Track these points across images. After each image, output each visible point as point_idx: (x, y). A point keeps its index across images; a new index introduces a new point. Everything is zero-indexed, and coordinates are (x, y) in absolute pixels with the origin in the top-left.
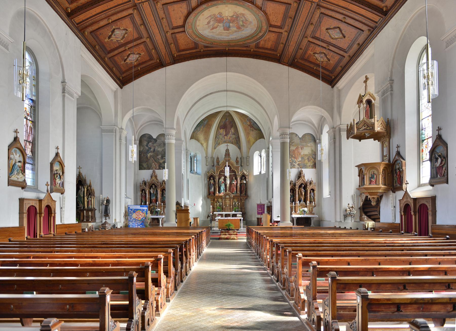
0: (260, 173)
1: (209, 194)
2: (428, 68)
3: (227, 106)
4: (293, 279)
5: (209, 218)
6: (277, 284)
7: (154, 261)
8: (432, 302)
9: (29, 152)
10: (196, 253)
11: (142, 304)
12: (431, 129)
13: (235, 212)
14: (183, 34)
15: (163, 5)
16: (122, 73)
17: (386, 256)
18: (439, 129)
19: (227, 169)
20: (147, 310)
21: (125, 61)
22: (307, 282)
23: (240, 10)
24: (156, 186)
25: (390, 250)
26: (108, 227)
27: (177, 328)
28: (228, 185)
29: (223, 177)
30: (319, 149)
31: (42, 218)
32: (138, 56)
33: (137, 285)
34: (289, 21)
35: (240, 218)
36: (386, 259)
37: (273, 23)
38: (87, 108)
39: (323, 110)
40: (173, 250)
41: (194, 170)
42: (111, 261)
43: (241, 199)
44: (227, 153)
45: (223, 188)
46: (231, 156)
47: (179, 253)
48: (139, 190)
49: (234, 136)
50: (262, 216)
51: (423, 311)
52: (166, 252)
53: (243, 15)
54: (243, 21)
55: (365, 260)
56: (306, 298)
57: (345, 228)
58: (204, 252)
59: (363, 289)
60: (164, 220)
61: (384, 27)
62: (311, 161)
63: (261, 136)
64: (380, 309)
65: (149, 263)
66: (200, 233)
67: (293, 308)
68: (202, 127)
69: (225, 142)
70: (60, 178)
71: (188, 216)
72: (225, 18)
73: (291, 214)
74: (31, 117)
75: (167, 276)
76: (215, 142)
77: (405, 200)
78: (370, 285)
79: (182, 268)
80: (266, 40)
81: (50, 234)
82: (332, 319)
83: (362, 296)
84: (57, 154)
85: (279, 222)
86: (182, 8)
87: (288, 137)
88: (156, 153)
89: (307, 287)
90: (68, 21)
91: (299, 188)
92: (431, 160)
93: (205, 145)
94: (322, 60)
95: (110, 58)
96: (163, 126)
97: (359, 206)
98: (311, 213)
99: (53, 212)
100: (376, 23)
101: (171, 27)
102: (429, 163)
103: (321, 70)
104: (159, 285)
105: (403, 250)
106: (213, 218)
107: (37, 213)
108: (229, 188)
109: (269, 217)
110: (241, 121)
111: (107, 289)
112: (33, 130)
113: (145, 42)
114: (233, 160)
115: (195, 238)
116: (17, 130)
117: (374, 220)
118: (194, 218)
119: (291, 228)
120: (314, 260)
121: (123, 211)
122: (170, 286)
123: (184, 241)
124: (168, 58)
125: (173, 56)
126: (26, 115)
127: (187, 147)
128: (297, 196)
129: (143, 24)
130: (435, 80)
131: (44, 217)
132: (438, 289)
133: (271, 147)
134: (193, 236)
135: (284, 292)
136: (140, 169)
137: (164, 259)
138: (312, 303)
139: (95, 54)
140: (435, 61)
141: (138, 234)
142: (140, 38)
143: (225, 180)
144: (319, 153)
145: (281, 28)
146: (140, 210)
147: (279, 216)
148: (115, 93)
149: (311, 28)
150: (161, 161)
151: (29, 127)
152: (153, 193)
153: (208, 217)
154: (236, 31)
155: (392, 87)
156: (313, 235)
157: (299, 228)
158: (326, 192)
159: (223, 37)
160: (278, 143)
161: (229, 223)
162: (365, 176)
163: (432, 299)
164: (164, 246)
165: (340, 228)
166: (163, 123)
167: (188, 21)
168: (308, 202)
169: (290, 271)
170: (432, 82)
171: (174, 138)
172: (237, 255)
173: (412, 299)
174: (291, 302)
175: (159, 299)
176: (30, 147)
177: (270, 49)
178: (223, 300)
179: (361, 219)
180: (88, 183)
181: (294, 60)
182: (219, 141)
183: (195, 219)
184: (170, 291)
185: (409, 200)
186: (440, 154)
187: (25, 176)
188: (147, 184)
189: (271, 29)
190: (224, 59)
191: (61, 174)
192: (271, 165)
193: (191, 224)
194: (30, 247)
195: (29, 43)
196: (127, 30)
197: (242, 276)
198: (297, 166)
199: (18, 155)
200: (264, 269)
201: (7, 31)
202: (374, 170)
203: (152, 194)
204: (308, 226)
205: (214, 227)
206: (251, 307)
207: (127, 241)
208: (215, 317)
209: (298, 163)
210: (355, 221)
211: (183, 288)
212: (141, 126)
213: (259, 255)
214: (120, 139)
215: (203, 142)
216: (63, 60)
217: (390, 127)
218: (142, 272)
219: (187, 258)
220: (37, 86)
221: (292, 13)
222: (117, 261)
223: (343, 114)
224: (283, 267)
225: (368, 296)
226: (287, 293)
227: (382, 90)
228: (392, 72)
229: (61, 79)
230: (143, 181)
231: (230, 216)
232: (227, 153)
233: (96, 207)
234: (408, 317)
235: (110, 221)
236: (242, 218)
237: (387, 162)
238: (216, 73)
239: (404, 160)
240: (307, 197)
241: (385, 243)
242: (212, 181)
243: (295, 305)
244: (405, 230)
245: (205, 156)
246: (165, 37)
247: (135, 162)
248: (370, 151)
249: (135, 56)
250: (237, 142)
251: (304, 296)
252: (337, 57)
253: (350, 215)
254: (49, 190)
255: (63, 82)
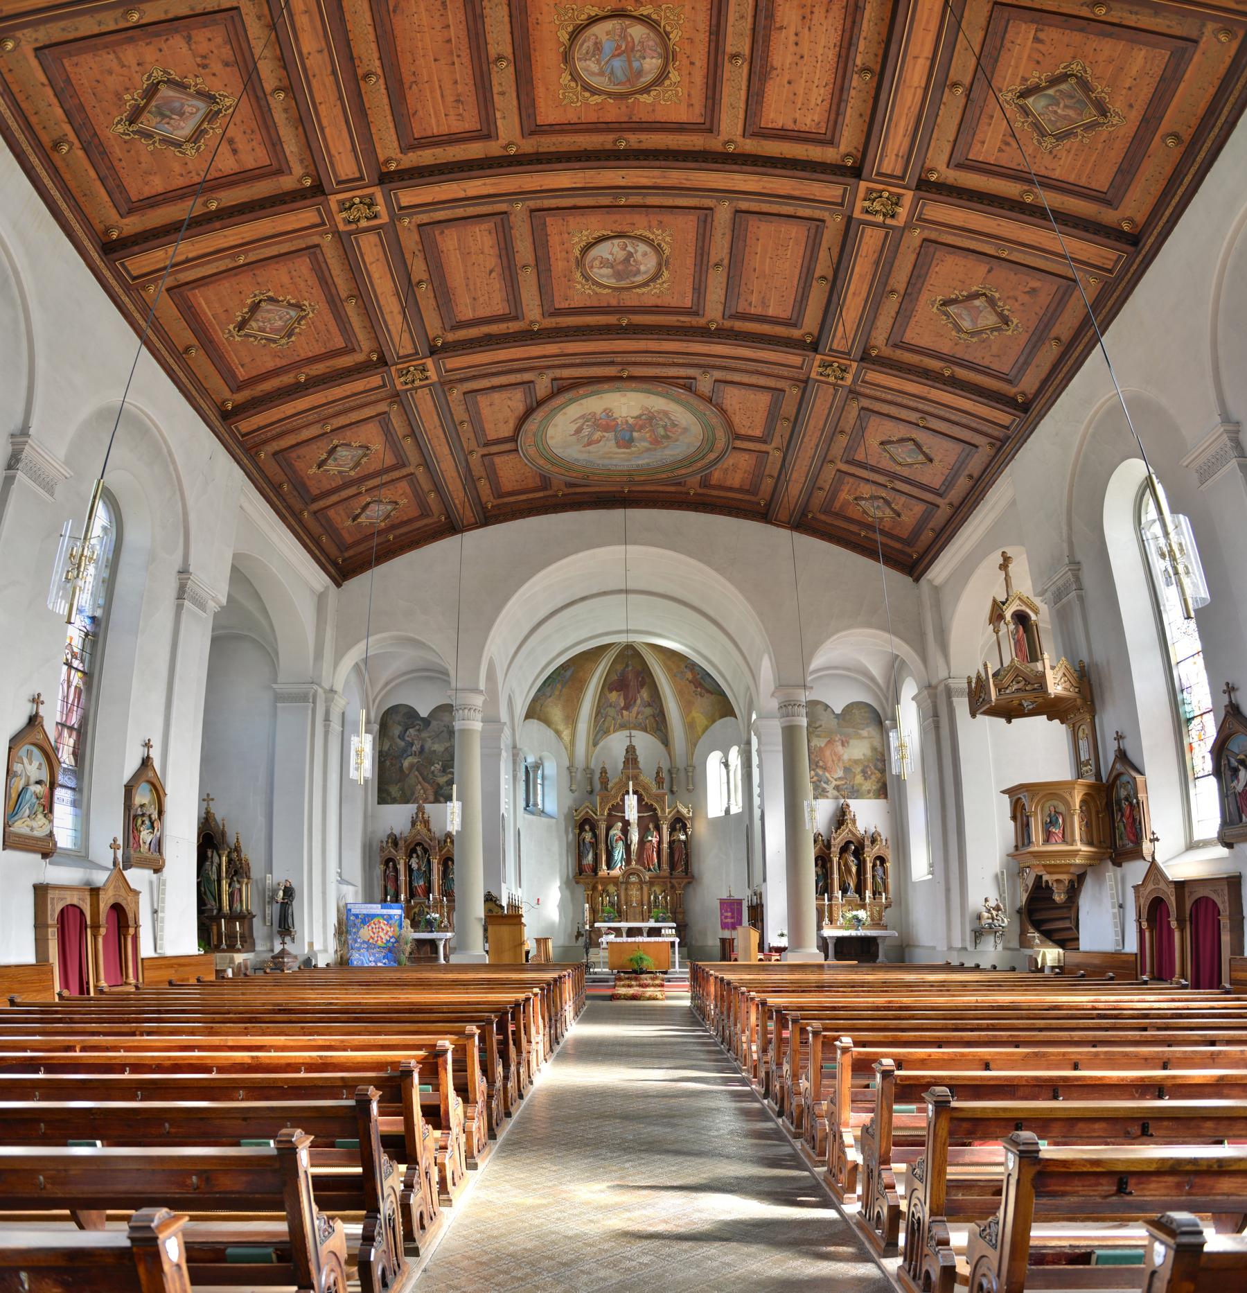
0: (727, 811)
1: (580, 870)
2: (1166, 534)
3: (627, 631)
4: (825, 1107)
5: (582, 940)
6: (780, 1121)
7: (426, 1058)
8: (1221, 1168)
9: (66, 757)
10: (547, 1038)
11: (401, 1175)
12: (1207, 689)
13: (657, 921)
14: (512, 456)
15: (465, 393)
16: (343, 547)
17: (1094, 1044)
18: (1230, 689)
19: (631, 802)
20: (415, 1190)
21: (354, 520)
22: (866, 1118)
23: (657, 403)
24: (425, 851)
25: (1107, 1029)
26: (292, 966)
27: (502, 1235)
28: (634, 847)
29: (620, 824)
30: (894, 743)
31: (100, 940)
32: (389, 507)
33: (382, 1123)
34: (783, 428)
35: (672, 939)
36: (1097, 1054)
37: (743, 432)
38: (240, 637)
39: (896, 640)
40: (478, 1027)
41: (536, 804)
42: (305, 1058)
43: (673, 887)
44: (631, 756)
45: (619, 853)
46: (641, 765)
47: (495, 1038)
48: (378, 859)
49: (648, 711)
50: (734, 934)
51: (1189, 1194)
52: (460, 1033)
53: (666, 413)
54: (665, 427)
55: (1036, 1054)
56: (859, 1159)
57: (978, 966)
58: (567, 1035)
59: (1026, 1135)
60: (452, 944)
61: (1029, 436)
62: (873, 777)
63: (725, 709)
64: (1068, 1188)
65: (413, 1062)
66: (555, 980)
67: (824, 1184)
68: (559, 686)
69: (623, 726)
70: (153, 827)
71: (520, 933)
72: (619, 421)
73: (820, 928)
74: (82, 661)
75: (466, 1101)
76: (595, 726)
77: (1151, 887)
78: (1044, 1124)
79: (506, 1078)
80: (727, 469)
81: (127, 984)
82: (932, 1213)
83: (1021, 1152)
84: (146, 762)
85: (784, 949)
86: (515, 402)
87: (804, 711)
88: (426, 757)
89: (865, 1129)
90: (221, 429)
91: (841, 853)
92: (1217, 772)
93: (566, 734)
94: (879, 514)
95: (315, 513)
96: (449, 683)
97: (1018, 905)
98: (877, 923)
99: (131, 922)
100: (1007, 428)
101: (482, 441)
102: (1213, 781)
103: (878, 537)
104: (444, 1123)
105: (1145, 1029)
106: (591, 939)
107: (85, 925)
108: (639, 857)
109: (755, 936)
110: (669, 670)
111: (298, 1132)
112: (83, 696)
113: (412, 474)
114: (648, 778)
115: (542, 995)
116: (39, 695)
117: (1061, 944)
118: (538, 941)
119: (821, 966)
120: (886, 1055)
121: (333, 920)
122: (474, 1126)
123: (510, 1003)
124: (469, 513)
125: (484, 508)
126: (69, 657)
127: (514, 741)
128: (836, 876)
129: (412, 434)
130: (1191, 560)
131: (105, 938)
132: (1241, 1136)
133: (754, 740)
134: (536, 990)
135: (798, 1144)
136: (382, 801)
137: (454, 1051)
138: (876, 1173)
139: (278, 503)
140: (1181, 516)
141: (378, 983)
142: (401, 464)
143: (625, 831)
144: (894, 756)
145: (765, 442)
146: (382, 916)
147: (785, 932)
148: (321, 598)
149: (842, 441)
150: (442, 780)
151: (72, 689)
152: (419, 869)
153: (577, 938)
154: (648, 450)
155: (1078, 579)
156: (885, 987)
157: (843, 966)
158: (920, 864)
159: (614, 462)
160: (774, 729)
161: (640, 953)
162: (1032, 820)
163: (1220, 1162)
164: (455, 1017)
165: (961, 968)
166: (448, 675)
167: (525, 427)
168: (868, 894)
169: (817, 1086)
170: (1186, 567)
171: (479, 716)
172: (665, 1044)
173: (1163, 1160)
174: (816, 1169)
175: (447, 1162)
176: (71, 742)
177: (740, 490)
178: (627, 1165)
179: (1024, 942)
180: (232, 840)
181: (804, 514)
182: (606, 724)
183: (542, 942)
184: (475, 1141)
185: (1162, 885)
186: (1242, 757)
187: (51, 821)
188: (401, 843)
189: (739, 444)
190: (617, 515)
191: (155, 816)
192: (756, 790)
193: (530, 956)
194: (72, 1021)
195: (111, 480)
196: (368, 448)
197: (677, 1100)
198: (831, 792)
199: (36, 764)
200: (743, 1082)
201: (61, 451)
202: (1055, 803)
203: (414, 870)
204: (868, 962)
205: (595, 965)
206: (704, 1181)
207: (347, 1004)
208: (608, 1209)
209: (835, 783)
210: (1004, 948)
211: (512, 1133)
212: (387, 684)
213: (729, 1042)
214: (327, 719)
215: (561, 727)
216: (192, 518)
217: (1090, 685)
218: (395, 1088)
219: (519, 1052)
220: (109, 585)
221: (788, 408)
222: (321, 1057)
223: (954, 648)
224: (795, 1077)
225: (1038, 1151)
226: (807, 1147)
227: (1054, 588)
228: (1071, 545)
229: (178, 565)
230: (389, 836)
231: (642, 935)
232: (631, 756)
233: (254, 909)
234: (1144, 1211)
235: (298, 948)
236: (677, 940)
237: (1092, 780)
238: (599, 546)
239: (1142, 774)
240: (865, 879)
241: (1094, 1009)
242: (588, 835)
243: (830, 1177)
244: (1152, 972)
245: (567, 764)
246: (464, 464)
247: (366, 781)
248: (1039, 750)
249: (382, 507)
250: (659, 725)
251: (854, 1155)
252: (919, 508)
253: (992, 930)
254: (120, 859)
255: (184, 572)
